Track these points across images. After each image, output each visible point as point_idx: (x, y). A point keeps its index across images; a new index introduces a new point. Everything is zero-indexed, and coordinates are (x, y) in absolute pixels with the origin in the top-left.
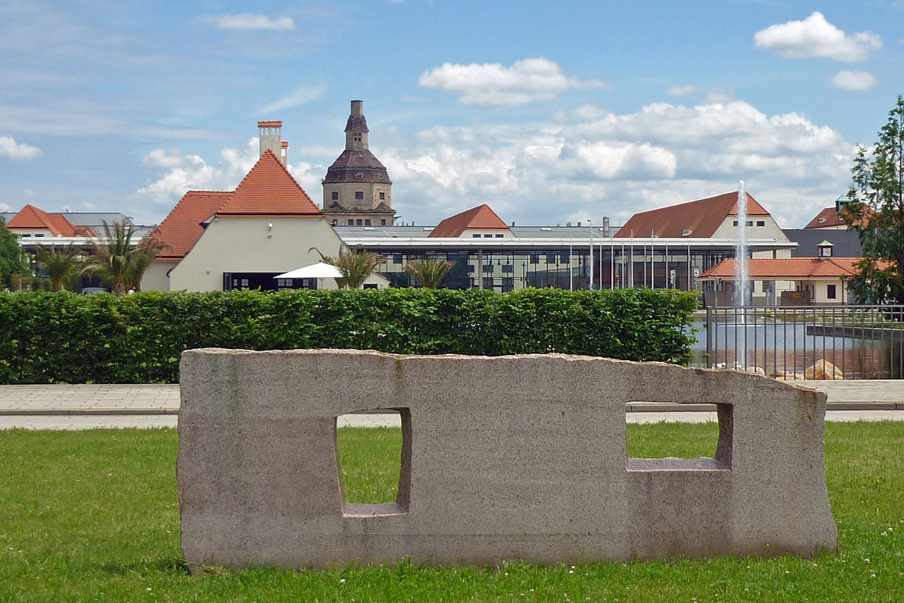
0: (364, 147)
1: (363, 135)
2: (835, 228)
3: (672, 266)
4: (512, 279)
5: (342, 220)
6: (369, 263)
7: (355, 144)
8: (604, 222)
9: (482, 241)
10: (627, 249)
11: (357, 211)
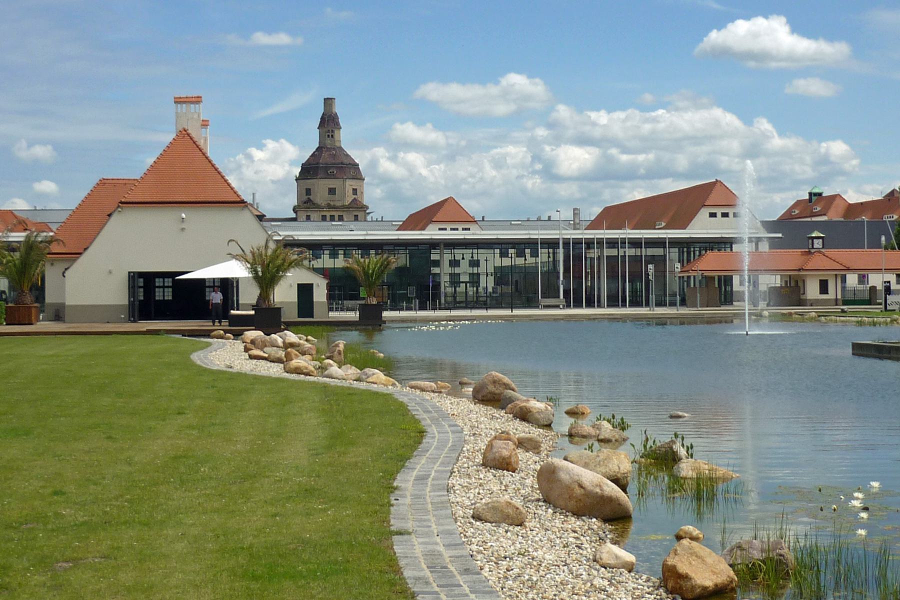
0: (337, 144)
1: (336, 132)
2: (809, 219)
3: (652, 259)
4: (478, 274)
5: (314, 216)
6: (284, 260)
7: (328, 142)
8: (574, 214)
9: (449, 235)
10: (600, 242)
11: (329, 207)
